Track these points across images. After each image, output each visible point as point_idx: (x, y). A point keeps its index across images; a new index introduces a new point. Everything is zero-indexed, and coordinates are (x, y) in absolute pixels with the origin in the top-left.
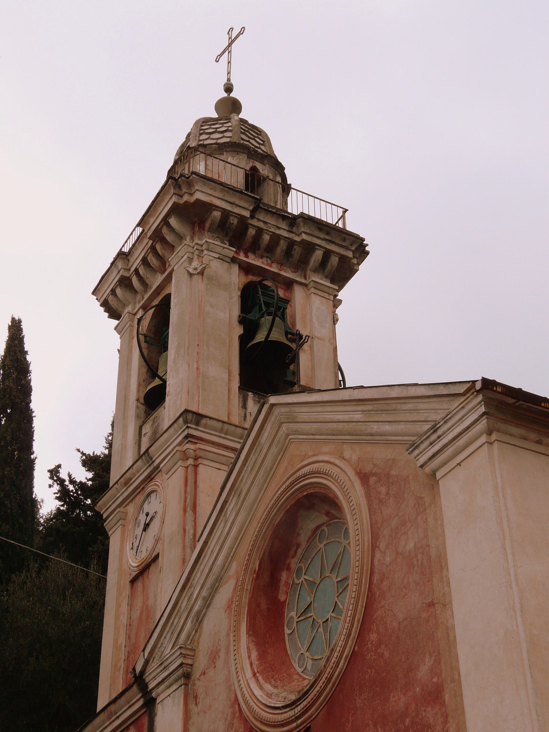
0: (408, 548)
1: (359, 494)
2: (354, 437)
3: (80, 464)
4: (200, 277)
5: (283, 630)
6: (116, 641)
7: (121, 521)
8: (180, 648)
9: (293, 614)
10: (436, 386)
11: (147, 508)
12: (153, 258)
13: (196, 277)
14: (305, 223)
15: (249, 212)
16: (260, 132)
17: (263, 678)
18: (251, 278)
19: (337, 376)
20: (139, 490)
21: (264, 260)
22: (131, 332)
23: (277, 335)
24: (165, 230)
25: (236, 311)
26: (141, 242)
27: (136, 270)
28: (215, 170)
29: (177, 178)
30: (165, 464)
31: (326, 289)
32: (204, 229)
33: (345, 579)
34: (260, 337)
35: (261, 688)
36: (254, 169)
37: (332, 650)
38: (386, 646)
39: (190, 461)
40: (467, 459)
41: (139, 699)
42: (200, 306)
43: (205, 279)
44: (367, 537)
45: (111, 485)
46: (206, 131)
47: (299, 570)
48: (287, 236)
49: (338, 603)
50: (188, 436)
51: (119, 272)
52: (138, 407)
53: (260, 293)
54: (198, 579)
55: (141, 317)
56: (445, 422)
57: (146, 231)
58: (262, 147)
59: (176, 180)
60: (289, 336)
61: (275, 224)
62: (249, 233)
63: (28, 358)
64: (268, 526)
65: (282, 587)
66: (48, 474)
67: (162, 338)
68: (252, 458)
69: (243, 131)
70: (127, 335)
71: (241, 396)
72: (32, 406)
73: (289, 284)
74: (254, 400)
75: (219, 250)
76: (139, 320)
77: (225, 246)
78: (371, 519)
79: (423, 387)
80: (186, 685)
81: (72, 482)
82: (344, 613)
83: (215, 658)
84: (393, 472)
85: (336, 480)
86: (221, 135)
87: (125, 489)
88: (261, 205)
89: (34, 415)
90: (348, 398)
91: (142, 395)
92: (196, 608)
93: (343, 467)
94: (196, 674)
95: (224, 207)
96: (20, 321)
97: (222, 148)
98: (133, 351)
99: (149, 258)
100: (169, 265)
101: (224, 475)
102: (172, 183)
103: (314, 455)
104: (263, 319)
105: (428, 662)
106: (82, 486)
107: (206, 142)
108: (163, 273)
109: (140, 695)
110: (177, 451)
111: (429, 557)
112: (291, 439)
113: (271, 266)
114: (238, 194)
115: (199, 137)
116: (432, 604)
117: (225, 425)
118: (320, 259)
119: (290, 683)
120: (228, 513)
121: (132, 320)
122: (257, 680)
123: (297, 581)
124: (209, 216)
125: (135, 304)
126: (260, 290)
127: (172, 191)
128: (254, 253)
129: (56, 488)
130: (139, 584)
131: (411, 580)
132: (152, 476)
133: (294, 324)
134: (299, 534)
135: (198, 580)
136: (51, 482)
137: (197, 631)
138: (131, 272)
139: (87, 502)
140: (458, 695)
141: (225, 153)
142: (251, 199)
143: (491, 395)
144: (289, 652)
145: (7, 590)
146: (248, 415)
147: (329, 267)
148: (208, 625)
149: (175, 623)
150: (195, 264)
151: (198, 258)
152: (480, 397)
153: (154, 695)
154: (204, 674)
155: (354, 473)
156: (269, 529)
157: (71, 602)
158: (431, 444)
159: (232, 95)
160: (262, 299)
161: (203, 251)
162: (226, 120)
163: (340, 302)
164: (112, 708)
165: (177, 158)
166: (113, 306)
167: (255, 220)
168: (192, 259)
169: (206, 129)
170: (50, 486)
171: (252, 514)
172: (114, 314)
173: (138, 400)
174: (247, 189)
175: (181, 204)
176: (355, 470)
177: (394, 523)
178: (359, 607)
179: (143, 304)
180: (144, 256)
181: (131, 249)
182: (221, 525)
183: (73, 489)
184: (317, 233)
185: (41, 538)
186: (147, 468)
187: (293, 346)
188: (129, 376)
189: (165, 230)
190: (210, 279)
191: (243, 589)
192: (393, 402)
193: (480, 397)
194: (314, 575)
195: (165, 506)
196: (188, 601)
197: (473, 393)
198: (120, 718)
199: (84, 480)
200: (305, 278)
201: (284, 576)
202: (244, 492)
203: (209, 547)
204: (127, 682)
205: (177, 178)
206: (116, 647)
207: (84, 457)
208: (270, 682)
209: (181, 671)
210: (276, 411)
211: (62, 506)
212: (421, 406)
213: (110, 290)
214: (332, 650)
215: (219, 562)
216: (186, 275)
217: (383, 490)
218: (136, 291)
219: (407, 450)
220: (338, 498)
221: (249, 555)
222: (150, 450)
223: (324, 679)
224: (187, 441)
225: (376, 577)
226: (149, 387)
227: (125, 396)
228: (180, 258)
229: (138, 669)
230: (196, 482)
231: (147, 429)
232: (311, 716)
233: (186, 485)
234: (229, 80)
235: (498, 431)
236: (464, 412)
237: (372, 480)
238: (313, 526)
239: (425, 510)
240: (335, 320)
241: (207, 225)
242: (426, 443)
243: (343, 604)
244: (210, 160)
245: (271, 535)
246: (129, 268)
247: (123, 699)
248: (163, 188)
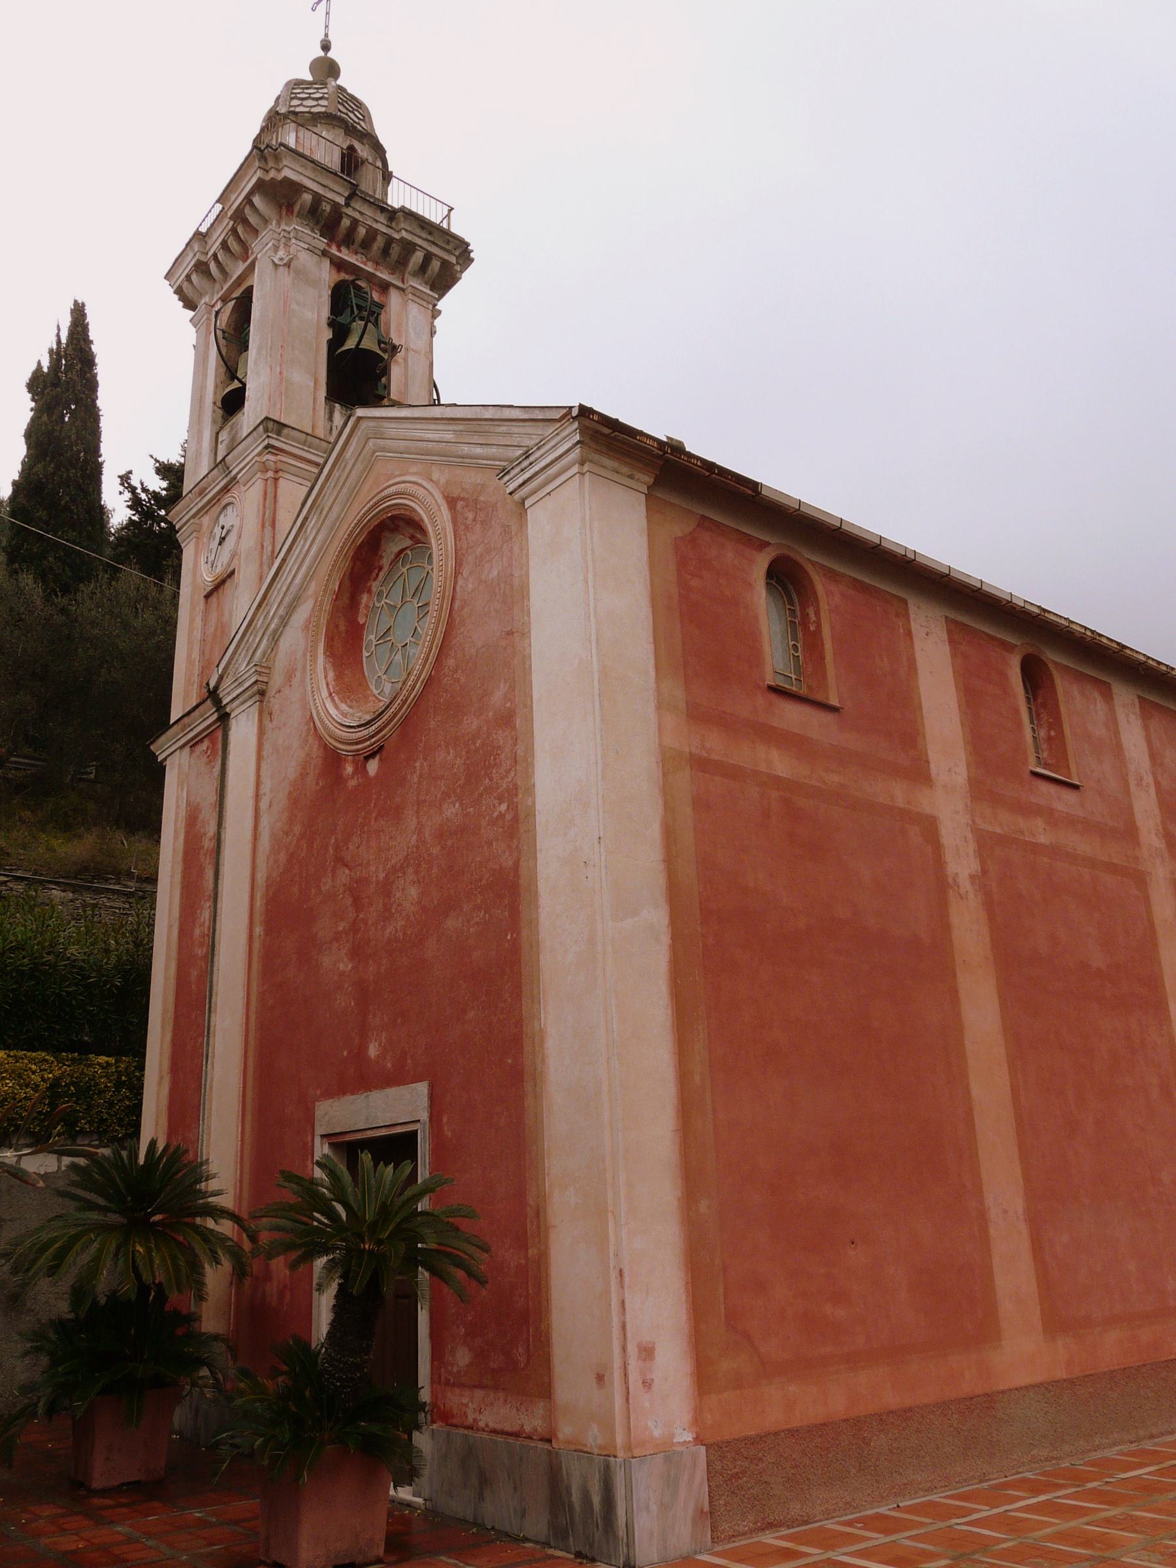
0: (491, 576)
1: (445, 517)
2: (443, 458)
3: (153, 471)
4: (287, 269)
5: (362, 652)
6: (189, 656)
7: (195, 533)
8: (255, 665)
9: (372, 637)
10: (531, 409)
11: (222, 520)
12: (234, 243)
13: (281, 268)
14: (405, 219)
15: (344, 199)
16: (360, 104)
17: (339, 699)
18: (343, 276)
19: (431, 394)
20: (214, 501)
21: (359, 256)
22: (208, 326)
23: (369, 344)
24: (248, 211)
25: (326, 312)
26: (221, 222)
27: (215, 256)
28: (307, 144)
29: (262, 148)
31: (425, 297)
32: (292, 213)
33: (426, 604)
34: (350, 344)
35: (337, 707)
36: (351, 148)
37: (409, 674)
38: (463, 672)
39: (270, 474)
41: (213, 713)
42: (285, 302)
43: (291, 271)
44: (452, 563)
45: (184, 495)
46: (298, 95)
47: (380, 594)
48: (385, 231)
49: (418, 628)
50: (268, 446)
51: (195, 255)
52: (214, 411)
53: (353, 294)
54: (275, 597)
55: (220, 310)
56: (538, 448)
57: (226, 209)
58: (362, 123)
59: (262, 151)
60: (382, 345)
61: (372, 216)
62: (342, 223)
63: (94, 348)
64: (350, 547)
65: (362, 610)
66: (119, 480)
67: (242, 336)
68: (336, 473)
69: (341, 101)
70: (203, 328)
71: (328, 407)
72: (99, 403)
73: (385, 287)
74: (341, 413)
75: (308, 239)
76: (217, 313)
77: (315, 236)
78: (456, 545)
79: (518, 410)
80: (261, 701)
81: (145, 490)
82: (423, 638)
83: (291, 676)
84: (482, 498)
85: (423, 503)
86: (315, 103)
87: (199, 499)
88: (357, 192)
89: (101, 413)
90: (440, 417)
91: (220, 398)
92: (273, 626)
93: (431, 490)
94: (271, 692)
95: (315, 190)
96: (83, 305)
97: (316, 118)
98: (210, 347)
99: (229, 242)
100: (252, 253)
101: (306, 490)
102: (257, 154)
103: (401, 475)
104: (355, 323)
105: (503, 688)
106: (155, 495)
107: (298, 109)
108: (245, 261)
109: (214, 709)
110: (256, 461)
111: (512, 586)
112: (377, 456)
113: (366, 264)
114: (332, 175)
115: (290, 102)
116: (510, 633)
117: (309, 437)
118: (421, 261)
119: (366, 704)
121: (209, 313)
122: (333, 700)
123: (377, 605)
124: (298, 199)
125: (213, 294)
126: (352, 290)
127: (257, 164)
128: (348, 247)
129: (128, 495)
130: (214, 599)
131: (492, 609)
132: (229, 487)
133: (388, 332)
134: (381, 557)
136: (121, 488)
137: (273, 649)
138: (209, 256)
139: (161, 513)
140: (529, 719)
141: (319, 125)
142: (346, 183)
143: (586, 422)
144: (366, 674)
145: (75, 600)
146: (334, 428)
147: (429, 272)
148: (285, 643)
149: (250, 641)
150: (281, 253)
151: (284, 247)
152: (576, 425)
153: (228, 710)
154: (280, 691)
155: (441, 496)
157: (142, 617)
158: (522, 470)
159: (330, 55)
160: (354, 301)
161: (290, 239)
162: (321, 84)
163: (439, 312)
164: (186, 720)
165: (264, 124)
166: (188, 295)
167: (350, 209)
168: (278, 247)
169: (299, 93)
170: (121, 493)
171: (333, 533)
172: (190, 304)
173: (215, 403)
174: (342, 172)
175: (267, 181)
176: (443, 493)
177: (479, 550)
178: (439, 633)
179: (222, 295)
180: (224, 239)
181: (209, 229)
182: (300, 542)
183: (146, 498)
184: (418, 231)
185: (112, 548)
186: (223, 479)
187: (386, 356)
188: (205, 376)
189: (248, 211)
190: (298, 272)
191: (321, 609)
192: (486, 423)
193: (576, 425)
194: (395, 599)
195: (242, 520)
197: (569, 420)
199: (157, 490)
200: (403, 282)
201: (365, 598)
202: (326, 509)
205: (262, 148)
206: (188, 681)
207: (157, 465)
208: (346, 702)
209: (256, 688)
210: (364, 425)
211: (134, 515)
212: (515, 430)
214: (409, 674)
215: (297, 581)
216: (271, 266)
217: (470, 515)
218: (214, 280)
219: (497, 475)
220: (423, 521)
221: (329, 575)
223: (399, 701)
224: (267, 451)
225: (457, 604)
226: (227, 390)
227: (201, 397)
229: (212, 685)
230: (275, 496)
231: (224, 436)
232: (385, 736)
233: (265, 499)
234: (326, 35)
235: (591, 461)
236: (558, 438)
237: (460, 504)
238: (396, 549)
239: (511, 538)
240: (433, 333)
241: (296, 208)
242: (517, 470)
243: (422, 629)
244: (302, 131)
245: (353, 556)
247: (197, 713)
248: (247, 159)
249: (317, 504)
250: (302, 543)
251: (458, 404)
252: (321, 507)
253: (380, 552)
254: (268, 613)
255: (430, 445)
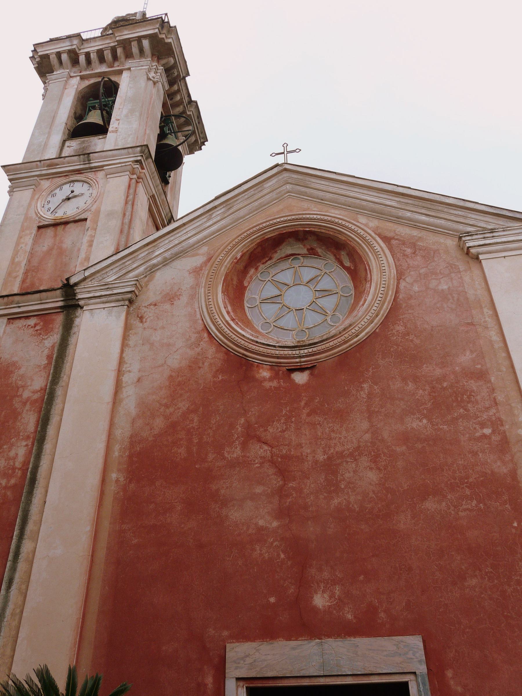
7: (34, 186)
8: (137, 280)
10: (502, 210)
30: (111, 168)
39: (135, 176)
40: (501, 258)
56: (504, 231)
68: (252, 192)
92: (155, 261)
108: (109, 67)
109: (62, 299)
120: (214, 215)
127: (158, 26)
132: (82, 172)
134: (276, 252)
135: (164, 245)
137: (146, 277)
149: (127, 264)
154: (155, 305)
156: (259, 238)
196: (147, 255)
198: (22, 308)
201: (252, 271)
203: (185, 229)
204: (21, 288)
209: (129, 296)
213: (57, 51)
222: (91, 155)
228: (140, 65)
232: (319, 359)
238: (289, 251)
246: (80, 48)
249: (228, 203)
250: (205, 220)
251: (412, 187)
252: (231, 206)
253: (277, 249)
254: (153, 252)
255: (364, 203)
